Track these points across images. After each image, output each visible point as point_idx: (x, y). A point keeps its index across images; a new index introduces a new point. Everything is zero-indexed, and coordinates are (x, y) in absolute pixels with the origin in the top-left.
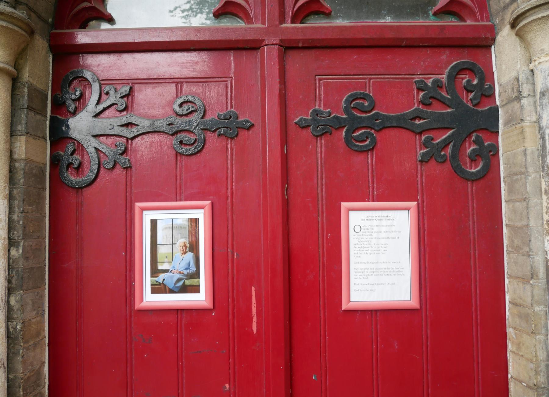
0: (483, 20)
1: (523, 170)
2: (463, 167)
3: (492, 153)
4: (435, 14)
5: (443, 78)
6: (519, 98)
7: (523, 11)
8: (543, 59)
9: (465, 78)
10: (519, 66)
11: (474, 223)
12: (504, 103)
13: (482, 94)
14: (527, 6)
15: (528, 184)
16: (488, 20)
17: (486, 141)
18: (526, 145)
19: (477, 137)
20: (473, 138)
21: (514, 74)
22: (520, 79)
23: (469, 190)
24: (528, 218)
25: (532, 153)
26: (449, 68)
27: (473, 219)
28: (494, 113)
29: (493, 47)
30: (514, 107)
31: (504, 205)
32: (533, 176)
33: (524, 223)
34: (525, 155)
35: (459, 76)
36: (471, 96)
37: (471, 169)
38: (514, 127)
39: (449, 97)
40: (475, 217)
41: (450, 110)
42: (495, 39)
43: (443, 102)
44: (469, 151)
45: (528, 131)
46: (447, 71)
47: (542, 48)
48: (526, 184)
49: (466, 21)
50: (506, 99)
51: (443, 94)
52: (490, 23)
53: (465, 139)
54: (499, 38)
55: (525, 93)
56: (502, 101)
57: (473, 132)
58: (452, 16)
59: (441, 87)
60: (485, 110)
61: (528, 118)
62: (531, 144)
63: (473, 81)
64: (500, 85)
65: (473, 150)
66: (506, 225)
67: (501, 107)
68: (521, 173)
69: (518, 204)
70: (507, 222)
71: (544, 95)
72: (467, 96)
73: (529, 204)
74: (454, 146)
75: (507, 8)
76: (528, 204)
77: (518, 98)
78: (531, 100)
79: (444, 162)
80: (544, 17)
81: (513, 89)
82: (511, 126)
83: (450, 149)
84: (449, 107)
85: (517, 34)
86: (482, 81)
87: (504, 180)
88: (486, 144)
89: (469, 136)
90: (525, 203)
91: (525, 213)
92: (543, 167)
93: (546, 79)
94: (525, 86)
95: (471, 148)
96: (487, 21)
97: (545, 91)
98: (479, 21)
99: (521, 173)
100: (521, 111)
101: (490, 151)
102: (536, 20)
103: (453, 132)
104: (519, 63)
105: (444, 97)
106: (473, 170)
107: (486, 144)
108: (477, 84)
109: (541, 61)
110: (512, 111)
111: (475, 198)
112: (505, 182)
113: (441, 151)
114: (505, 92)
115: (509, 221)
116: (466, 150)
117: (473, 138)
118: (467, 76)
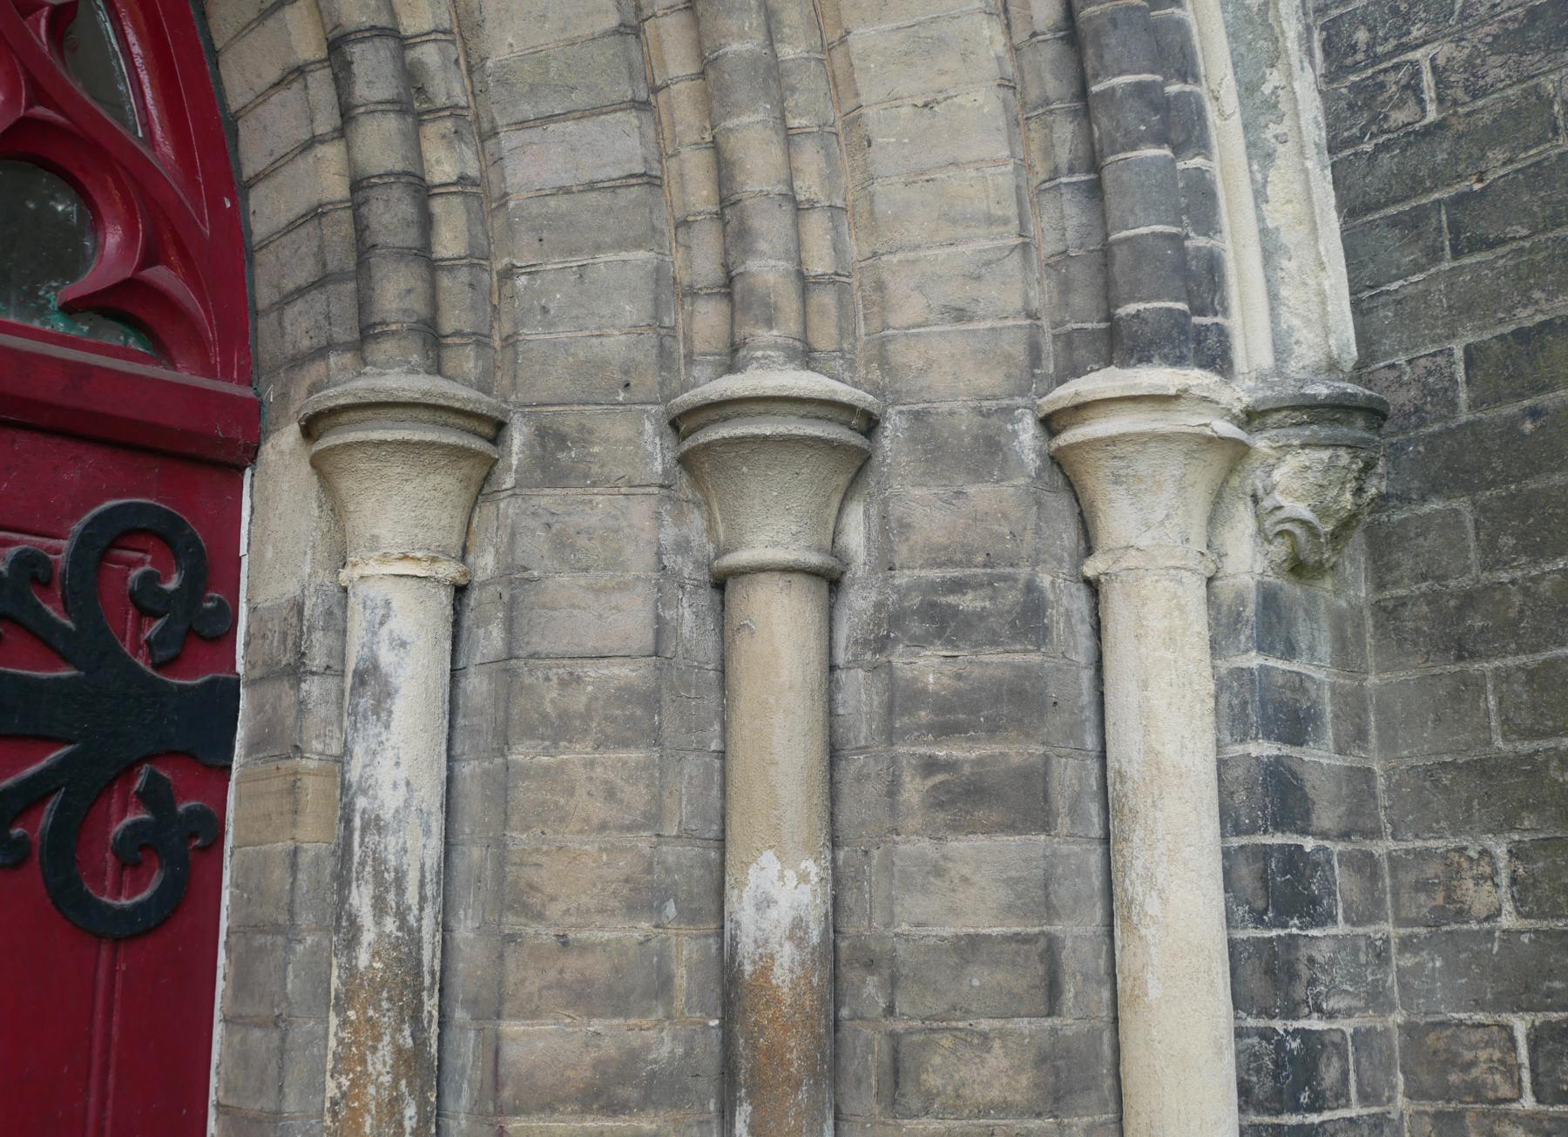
0: (227, 377)
1: (283, 919)
2: (86, 886)
3: (198, 842)
4: (70, 309)
5: (58, 552)
6: (296, 672)
7: (331, 404)
8: (373, 568)
9: (141, 562)
10: (307, 570)
11: (102, 1103)
12: (257, 673)
13: (190, 631)
14: (342, 394)
15: (290, 967)
16: (246, 379)
17: (185, 798)
18: (300, 834)
19: (153, 778)
20: (138, 784)
21: (291, 588)
22: (307, 613)
23: (102, 974)
24: (281, 1087)
25: (317, 861)
26: (87, 517)
27: (103, 1082)
28: (223, 698)
29: (248, 472)
30: (279, 697)
31: (218, 1030)
32: (309, 940)
33: (267, 1103)
34: (294, 867)
35: (117, 552)
36: (152, 629)
37: (117, 894)
38: (273, 766)
39: (69, 623)
40: (111, 1078)
41: (66, 673)
42: (257, 449)
43: (48, 643)
44: (117, 829)
45: (310, 784)
46: (77, 527)
47: (375, 531)
48: (285, 970)
49: (173, 365)
50: (265, 663)
51: (48, 608)
52: (250, 393)
53: (110, 784)
54: (268, 452)
55: (317, 660)
56: (253, 666)
57: (140, 762)
58: (121, 327)
59: (45, 585)
60: (193, 687)
61: (317, 746)
62: (313, 837)
63: (168, 578)
64: (253, 610)
65: (135, 824)
66: (218, 1105)
67: (252, 683)
68: (277, 929)
69: (257, 1034)
70: (221, 1094)
71: (363, 683)
72: (139, 630)
73: (289, 1039)
74: (63, 807)
75: (301, 367)
76: (283, 1040)
77: (295, 673)
78: (331, 683)
79: (17, 865)
80: (385, 442)
81: (285, 634)
82: (266, 761)
83: (46, 818)
84: (67, 660)
85: (316, 463)
86: (196, 583)
87: (226, 943)
88: (182, 808)
89: (129, 771)
90: (276, 1035)
91: (272, 1070)
92: (339, 919)
93: (374, 634)
94: (318, 636)
95: (129, 819)
96: (240, 383)
97: (366, 671)
98: (214, 376)
99: (277, 929)
100: (297, 718)
101: (194, 835)
102: (363, 443)
103: (67, 757)
104: (309, 557)
105: (53, 621)
106: (124, 902)
107: (182, 808)
108: (176, 590)
109: (367, 571)
110: (274, 709)
111: (117, 1006)
112: (228, 950)
113: (12, 825)
114: (264, 637)
115: (227, 1091)
116: (107, 822)
117: (138, 784)
118: (149, 558)
